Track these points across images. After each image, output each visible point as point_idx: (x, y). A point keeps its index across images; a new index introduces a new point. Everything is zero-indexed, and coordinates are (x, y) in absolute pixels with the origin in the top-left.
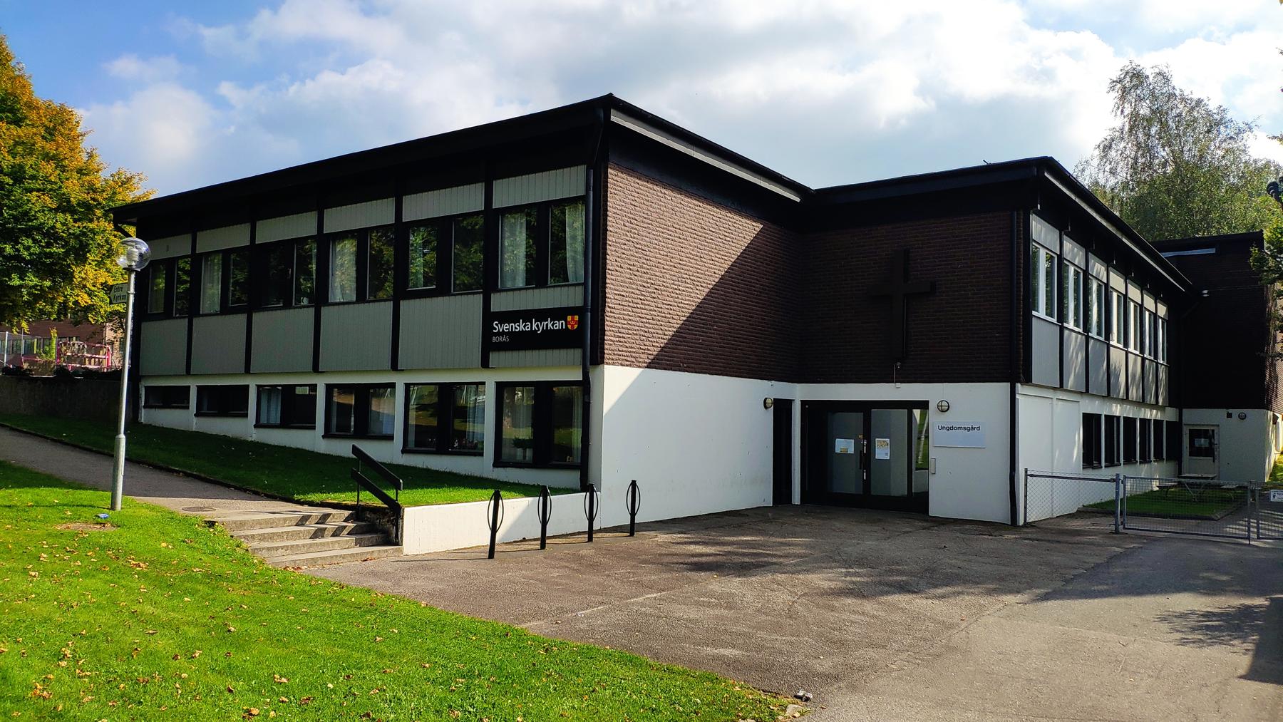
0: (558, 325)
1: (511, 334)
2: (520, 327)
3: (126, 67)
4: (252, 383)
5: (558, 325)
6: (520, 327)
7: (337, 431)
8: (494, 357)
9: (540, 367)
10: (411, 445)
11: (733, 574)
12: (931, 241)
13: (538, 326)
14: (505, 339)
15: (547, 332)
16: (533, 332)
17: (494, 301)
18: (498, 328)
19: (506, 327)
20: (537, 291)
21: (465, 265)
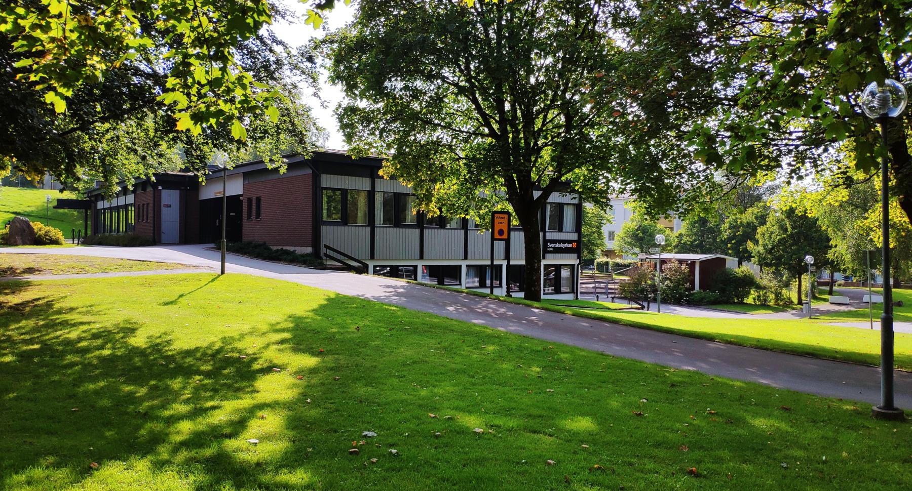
0: (570, 246)
1: (554, 248)
2: (557, 245)
3: (86, 475)
4: (464, 264)
5: (570, 246)
6: (557, 245)
7: (545, 265)
8: (547, 255)
9: (560, 259)
10: (458, 283)
11: (87, 373)
12: (619, 470)
13: (564, 246)
14: (552, 249)
15: (566, 248)
16: (561, 248)
17: (105, 267)
18: (549, 245)
19: (552, 245)
20: (395, 229)
21: (397, 149)
